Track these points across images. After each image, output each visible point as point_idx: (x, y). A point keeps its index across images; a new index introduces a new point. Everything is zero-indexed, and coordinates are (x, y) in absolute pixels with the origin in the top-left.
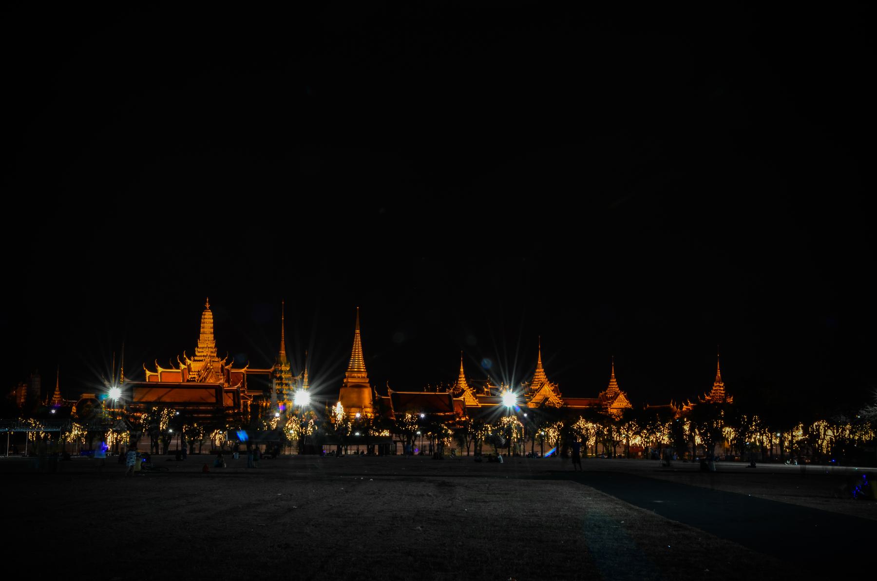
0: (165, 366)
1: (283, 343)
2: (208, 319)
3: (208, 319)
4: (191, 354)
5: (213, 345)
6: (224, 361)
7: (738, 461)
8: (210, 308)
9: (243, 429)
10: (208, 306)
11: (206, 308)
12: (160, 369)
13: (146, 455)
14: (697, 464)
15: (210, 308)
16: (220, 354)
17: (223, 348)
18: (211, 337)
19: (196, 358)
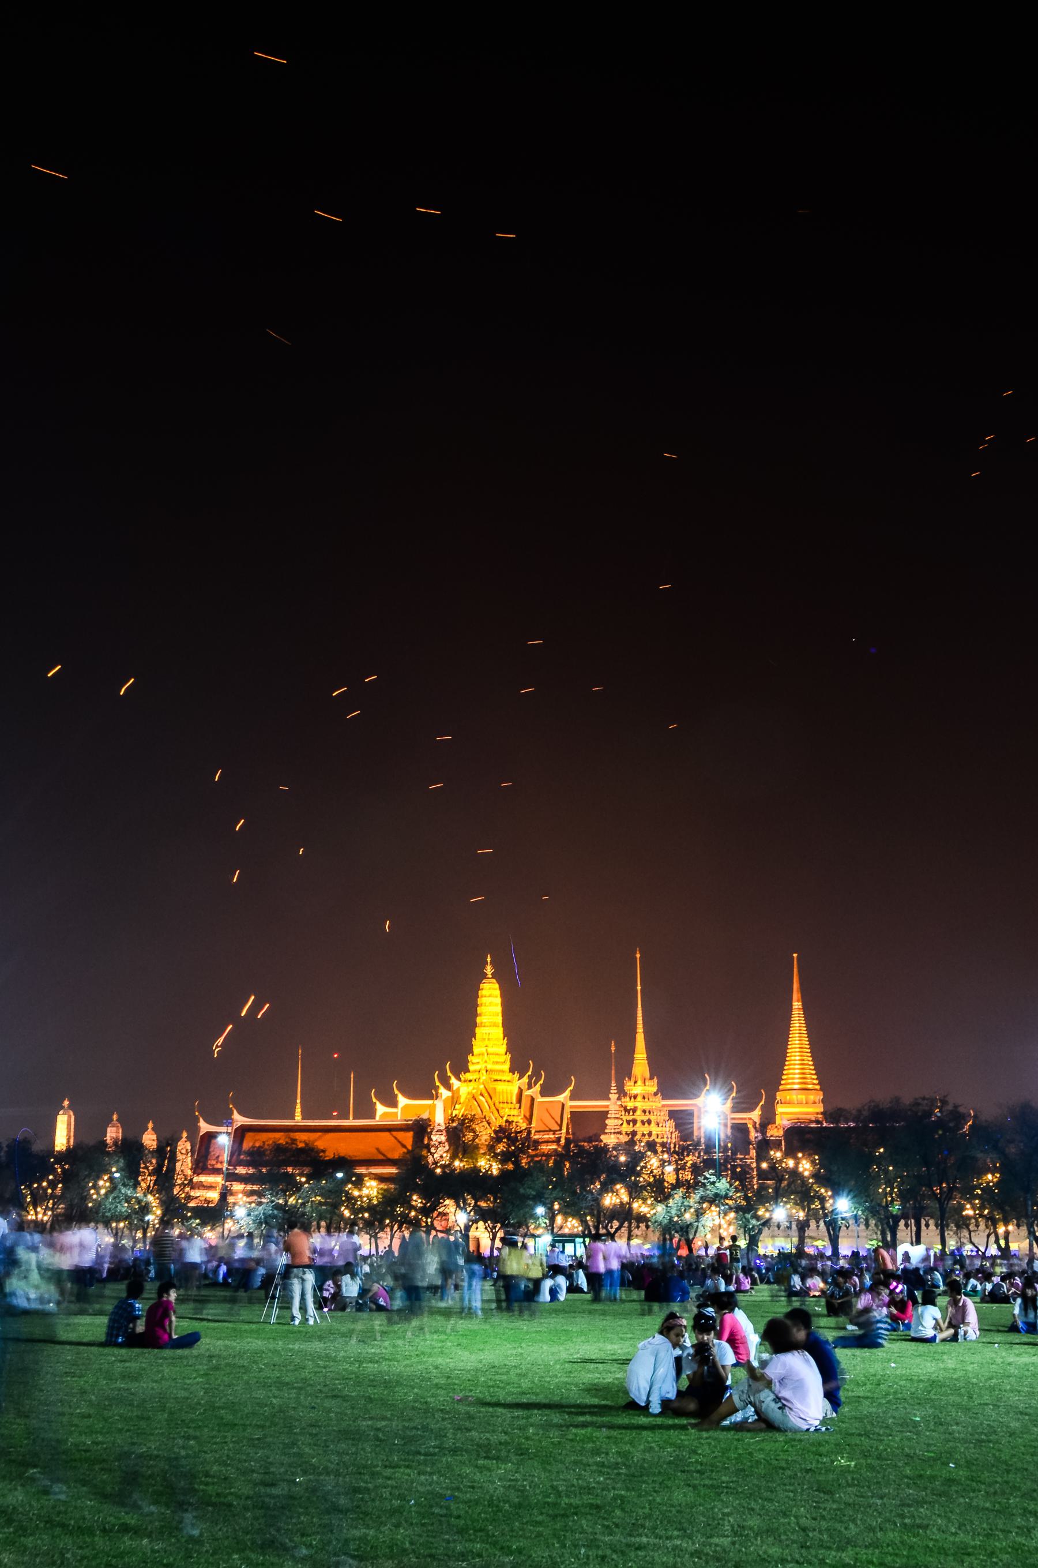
0: (410, 1094)
1: (796, 986)
2: (490, 1000)
3: (490, 1000)
4: (461, 1067)
5: (504, 1048)
6: (525, 1079)
7: (315, 1296)
8: (494, 976)
9: (484, 1258)
10: (489, 970)
11: (485, 976)
12: (402, 1101)
13: (746, 1209)
14: (723, 1497)
15: (494, 976)
16: (517, 1067)
17: (522, 1056)
18: (499, 1031)
19: (468, 1076)
